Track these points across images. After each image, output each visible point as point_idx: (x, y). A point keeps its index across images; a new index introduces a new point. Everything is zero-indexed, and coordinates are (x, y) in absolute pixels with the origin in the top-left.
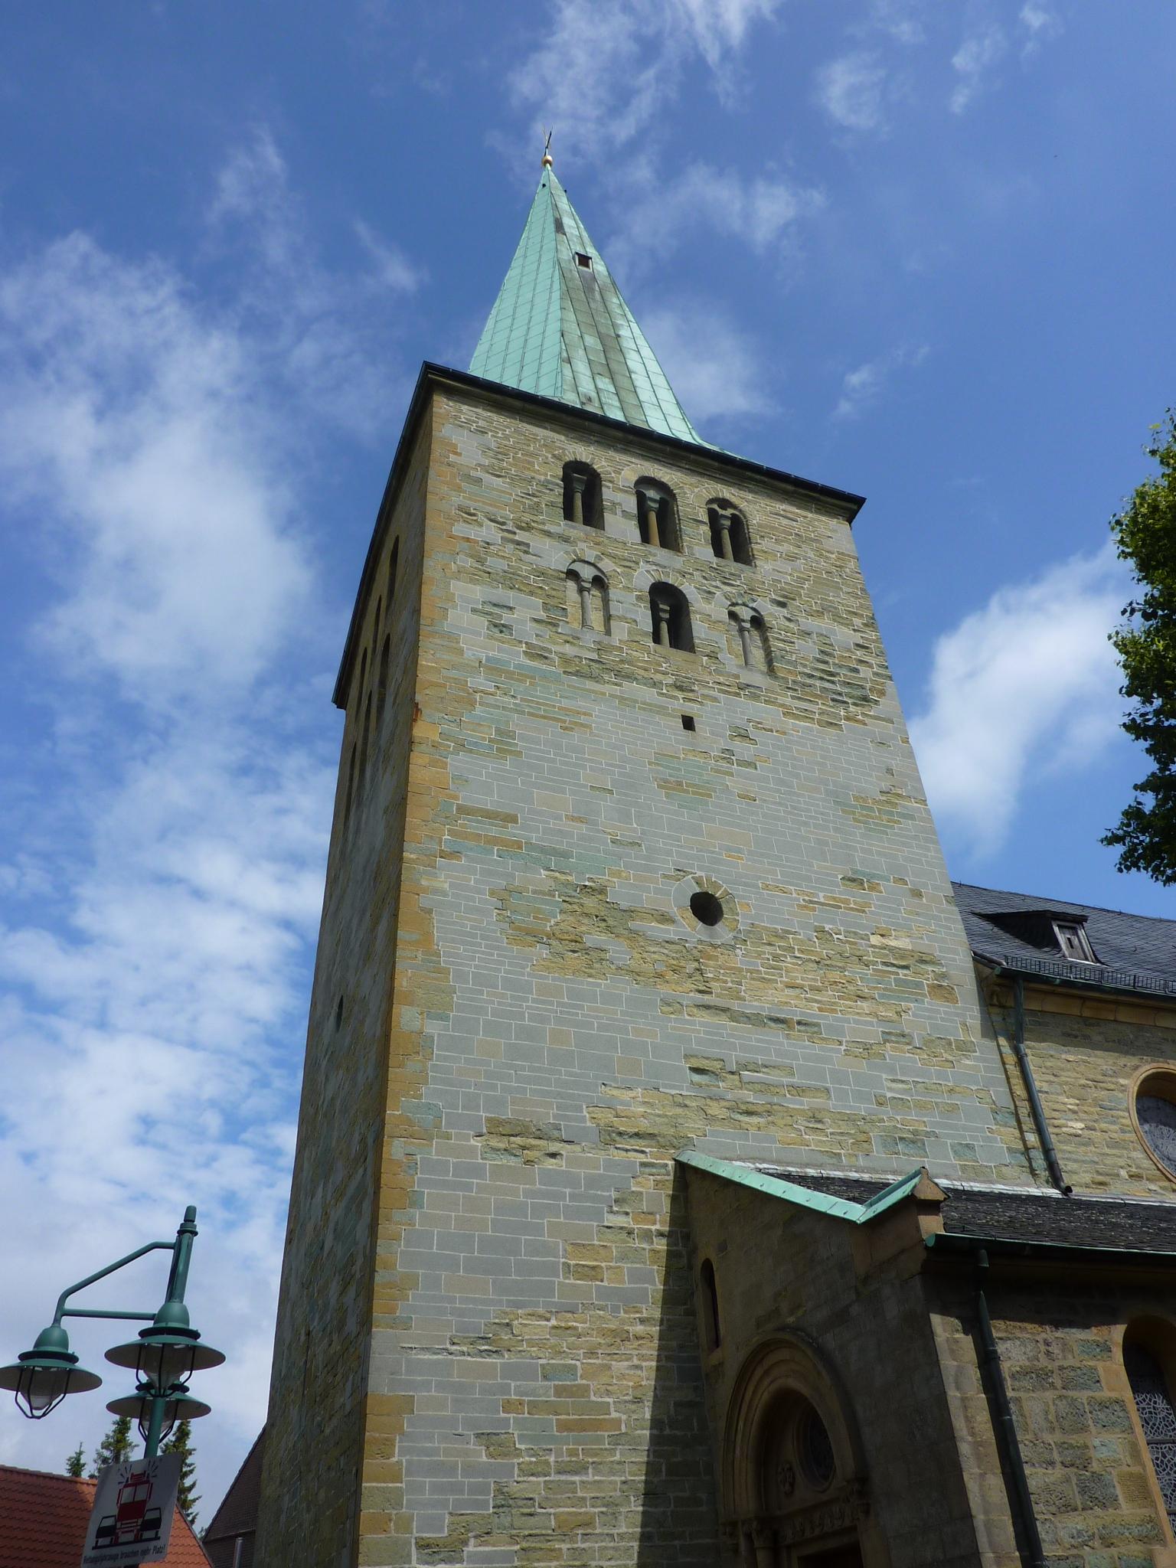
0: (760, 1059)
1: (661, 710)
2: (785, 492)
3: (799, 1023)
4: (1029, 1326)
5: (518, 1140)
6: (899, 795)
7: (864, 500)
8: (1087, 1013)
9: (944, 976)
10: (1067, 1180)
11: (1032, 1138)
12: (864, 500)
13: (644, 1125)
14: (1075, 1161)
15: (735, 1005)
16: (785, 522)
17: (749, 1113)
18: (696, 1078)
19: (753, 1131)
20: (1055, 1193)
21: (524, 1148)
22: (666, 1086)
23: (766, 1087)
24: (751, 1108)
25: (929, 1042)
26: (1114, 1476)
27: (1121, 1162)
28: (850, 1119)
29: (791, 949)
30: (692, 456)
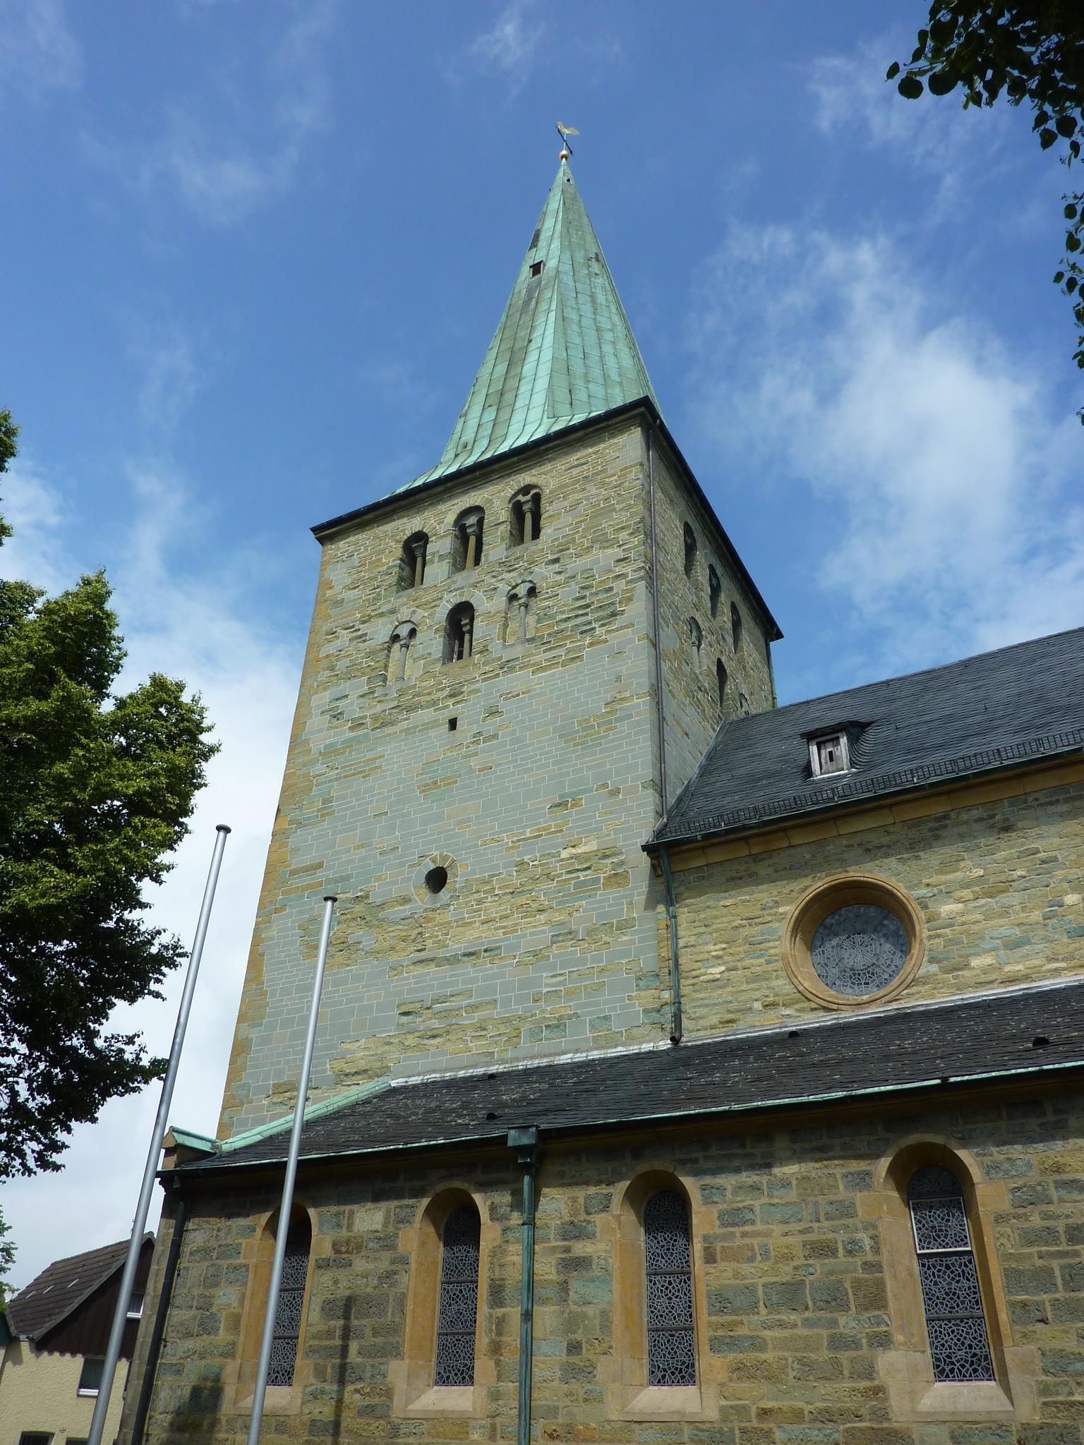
0: (449, 991)
2: (580, 440)
3: (486, 951)
4: (212, 1220)
5: (288, 1094)
6: (622, 699)
8: (755, 850)
9: (622, 863)
13: (362, 1065)
14: (706, 1006)
15: (441, 954)
17: (434, 1037)
18: (404, 1019)
19: (433, 1050)
22: (381, 1032)
24: (435, 1032)
25: (591, 932)
26: (223, 1317)
27: (757, 995)
28: (508, 1021)
30: (496, 466)
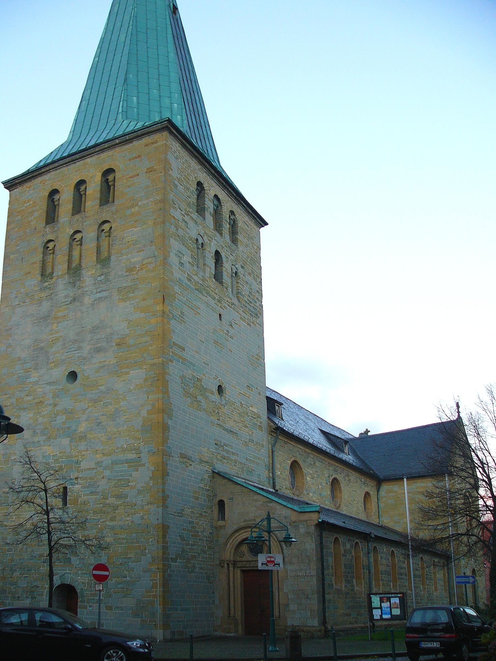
1: (213, 309)
5: (185, 460)
7: (266, 224)
10: (277, 488)
11: (271, 475)
12: (266, 224)
15: (224, 425)
16: (246, 227)
17: (224, 459)
20: (274, 491)
21: (186, 462)
23: (228, 452)
29: (235, 408)
